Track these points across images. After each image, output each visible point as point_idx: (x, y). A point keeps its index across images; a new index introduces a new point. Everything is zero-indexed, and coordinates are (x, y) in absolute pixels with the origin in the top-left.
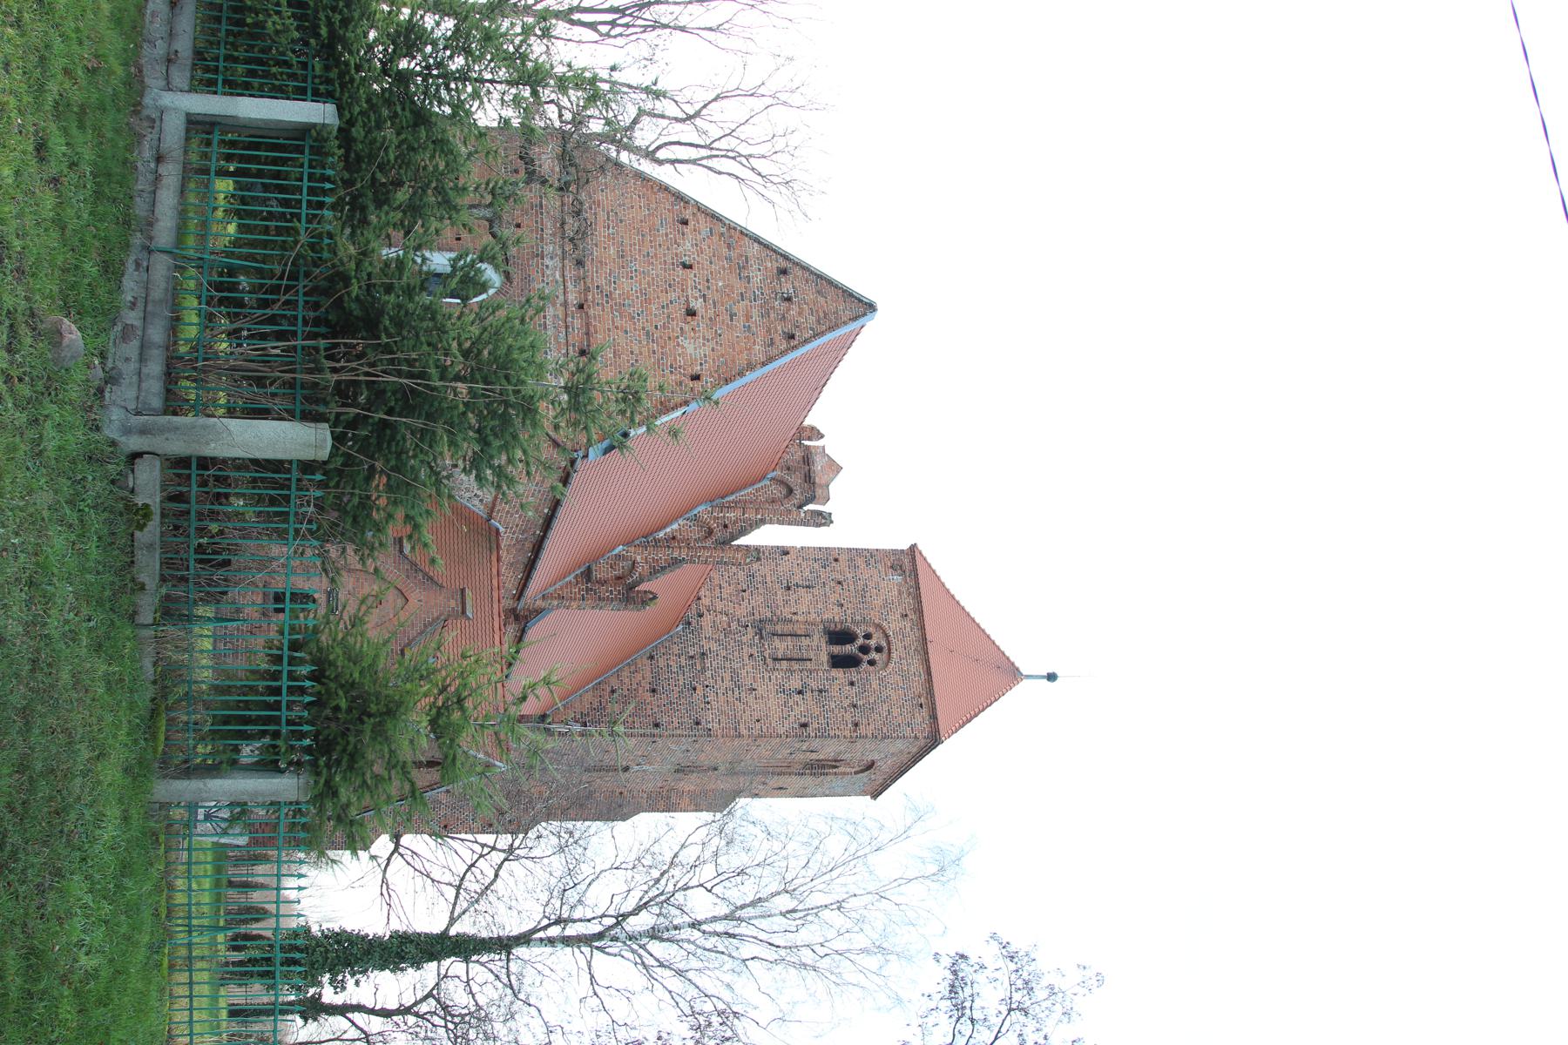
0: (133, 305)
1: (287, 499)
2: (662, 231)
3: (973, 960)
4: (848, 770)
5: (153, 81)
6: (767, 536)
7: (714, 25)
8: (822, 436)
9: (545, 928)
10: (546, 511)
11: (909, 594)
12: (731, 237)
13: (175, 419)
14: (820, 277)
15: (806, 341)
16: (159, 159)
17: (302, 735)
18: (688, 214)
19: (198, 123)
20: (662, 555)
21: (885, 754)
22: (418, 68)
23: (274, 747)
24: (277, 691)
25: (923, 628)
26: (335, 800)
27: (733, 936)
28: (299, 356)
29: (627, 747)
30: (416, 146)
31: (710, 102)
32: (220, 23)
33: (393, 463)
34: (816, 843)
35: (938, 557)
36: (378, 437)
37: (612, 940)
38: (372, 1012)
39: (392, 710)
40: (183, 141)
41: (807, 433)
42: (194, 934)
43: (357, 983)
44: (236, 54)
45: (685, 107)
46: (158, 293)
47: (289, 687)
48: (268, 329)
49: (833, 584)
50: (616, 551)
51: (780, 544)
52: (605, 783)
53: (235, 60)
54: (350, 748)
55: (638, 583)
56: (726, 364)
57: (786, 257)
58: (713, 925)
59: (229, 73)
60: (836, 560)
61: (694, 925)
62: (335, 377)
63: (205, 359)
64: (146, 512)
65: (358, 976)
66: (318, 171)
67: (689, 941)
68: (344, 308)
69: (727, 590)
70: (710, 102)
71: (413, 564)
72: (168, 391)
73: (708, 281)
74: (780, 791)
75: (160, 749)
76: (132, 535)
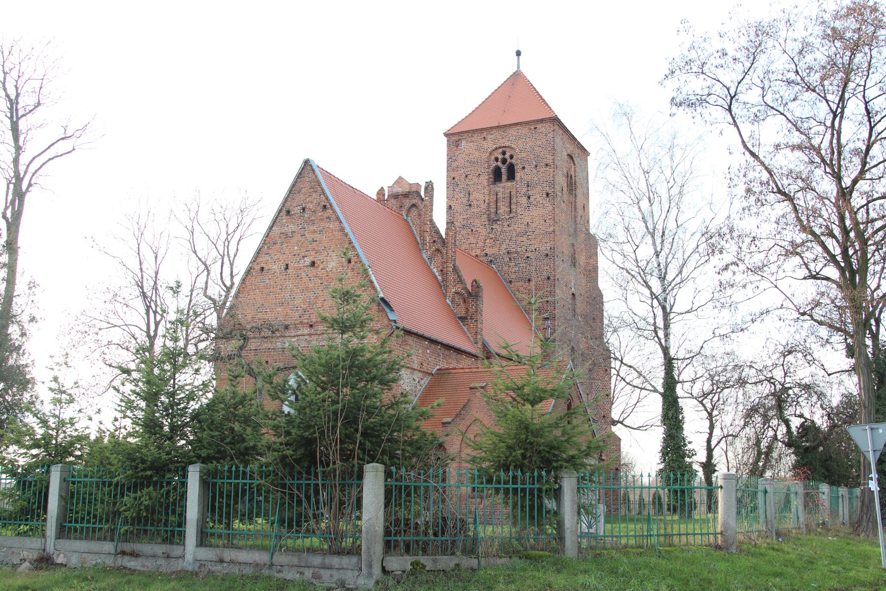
0: (301, 573)
1: (407, 487)
2: (268, 281)
3: (674, 94)
4: (573, 169)
5: (179, 565)
6: (440, 218)
7: (154, 255)
8: (382, 188)
9: (659, 339)
10: (427, 343)
11: (472, 136)
13: (363, 549)
14: (291, 191)
15: (327, 198)
16: (222, 561)
17: (540, 476)
18: (258, 267)
19: (201, 540)
20: (451, 277)
21: (563, 148)
22: (169, 420)
23: (546, 491)
24: (515, 490)
25: (491, 128)
26: (576, 457)
27: (663, 233)
28: (328, 482)
29: (561, 294)
30: (210, 420)
31: (197, 256)
32: (147, 530)
33: (386, 428)
34: (611, 187)
35: (450, 122)
36: (372, 437)
37: (666, 301)
38: (711, 434)
39: (524, 426)
40: (211, 549)
41: (381, 196)
42: (652, 533)
43: (690, 443)
44: (163, 521)
45: (200, 271)
46: (295, 560)
47: (513, 484)
48: (313, 500)
49: (467, 180)
50: (450, 303)
51: (445, 210)
52: (581, 306)
53: (167, 521)
54: (546, 449)
55: (466, 289)
56: (341, 244)
57: (280, 211)
58: (657, 244)
59: (174, 524)
60: (454, 178)
61: (657, 254)
62: (338, 462)
63: (331, 534)
64: (415, 564)
65: (686, 442)
66: (226, 474)
67: (667, 258)
68: (300, 458)
69: (472, 240)
70: (197, 256)
71: (457, 416)
72: (348, 553)
73: (295, 255)
74: (585, 207)
75: (548, 554)
76: (428, 571)
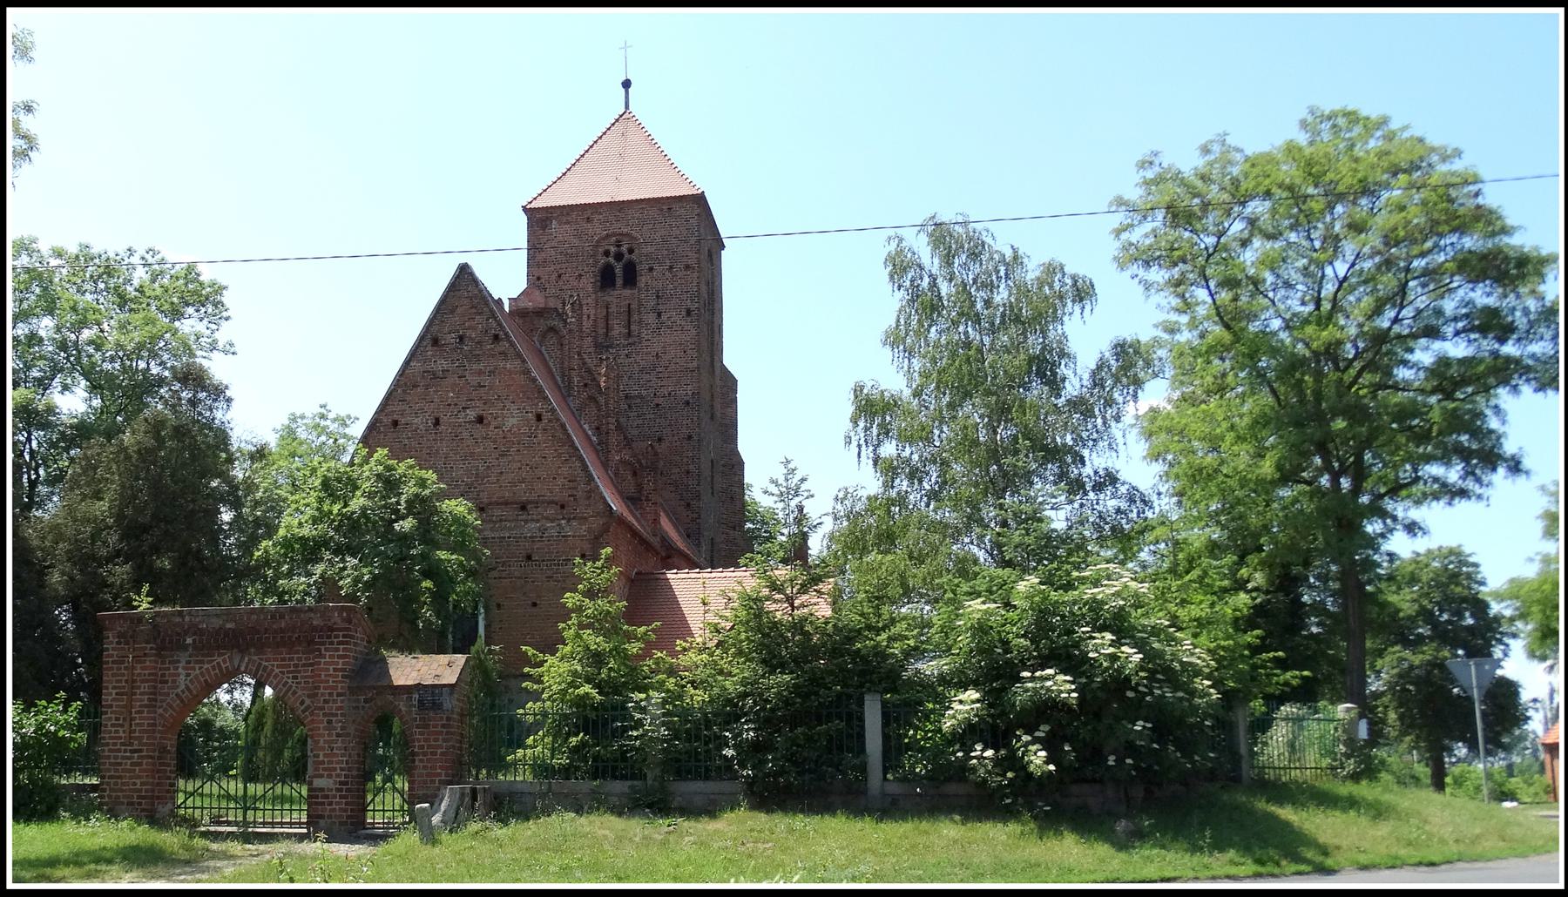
12: (406, 384)
15: (500, 324)
49: (561, 283)
60: (539, 279)
73: (449, 405)
